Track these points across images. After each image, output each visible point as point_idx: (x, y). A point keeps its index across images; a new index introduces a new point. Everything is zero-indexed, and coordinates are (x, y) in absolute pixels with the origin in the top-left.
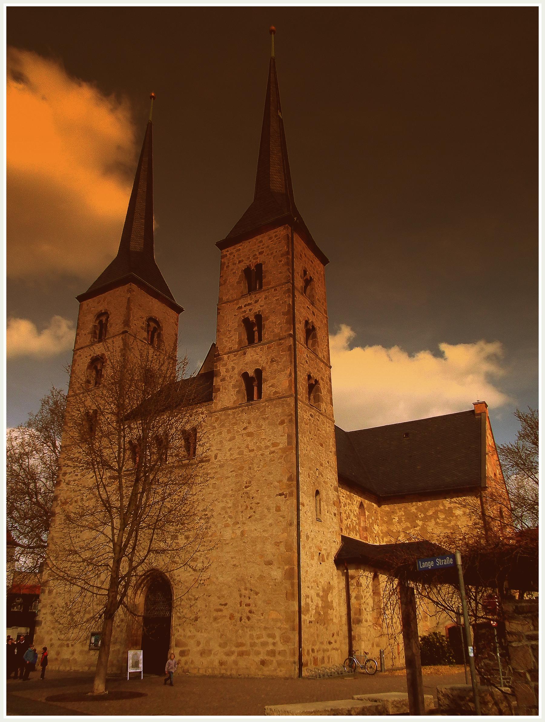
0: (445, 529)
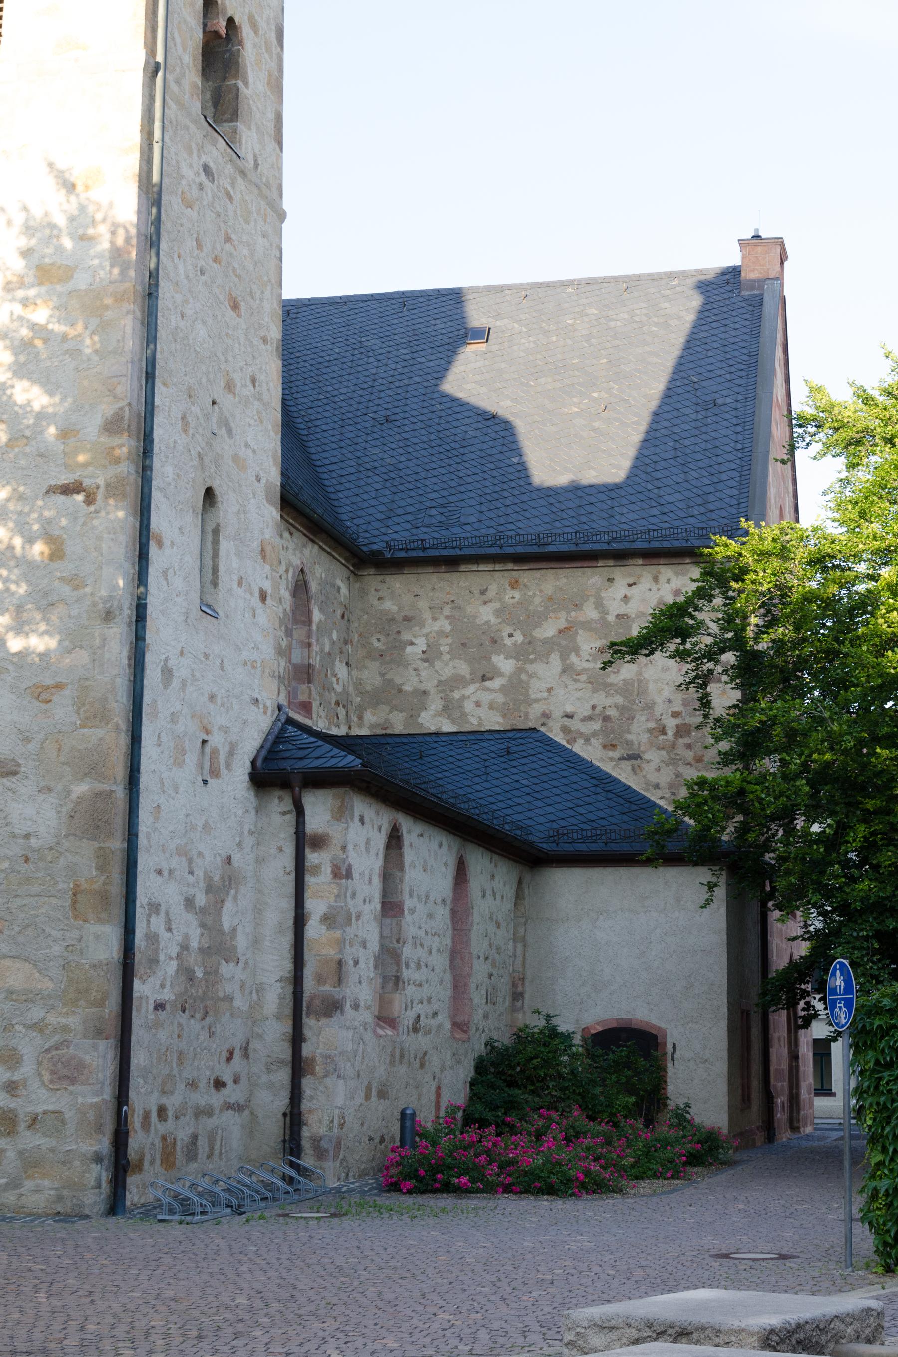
0: (595, 691)
